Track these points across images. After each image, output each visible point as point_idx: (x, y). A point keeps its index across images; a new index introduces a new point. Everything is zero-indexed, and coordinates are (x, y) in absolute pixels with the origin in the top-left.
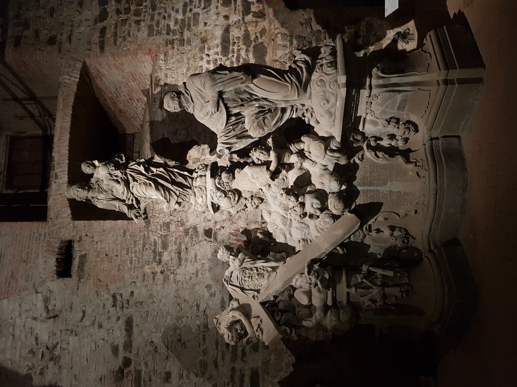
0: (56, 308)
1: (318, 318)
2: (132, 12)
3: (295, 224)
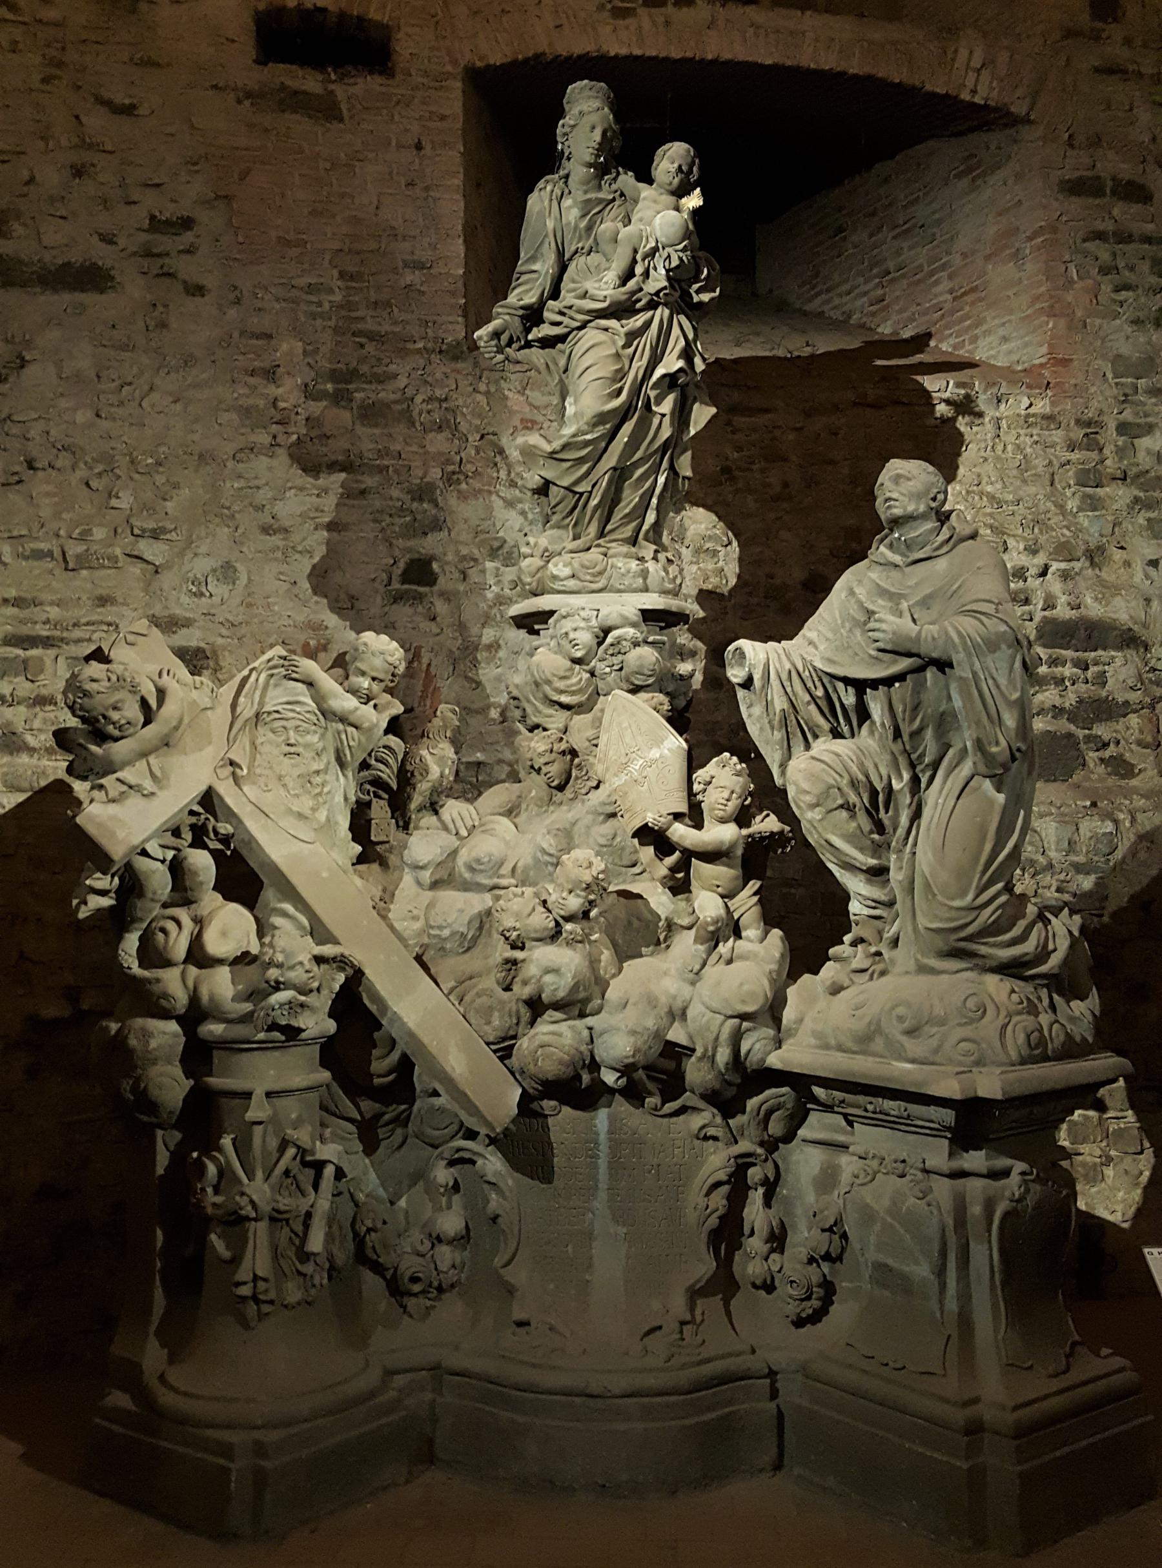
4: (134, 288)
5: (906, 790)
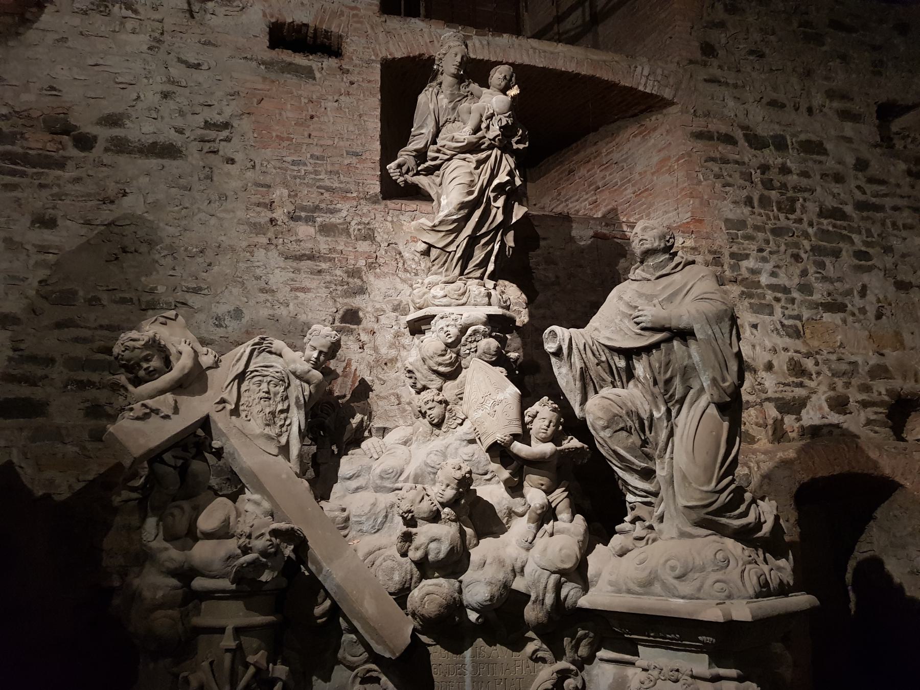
0: (209, 16)
1: (164, 556)
2: (766, 193)
3: (385, 499)
4: (194, 157)
5: (664, 417)
